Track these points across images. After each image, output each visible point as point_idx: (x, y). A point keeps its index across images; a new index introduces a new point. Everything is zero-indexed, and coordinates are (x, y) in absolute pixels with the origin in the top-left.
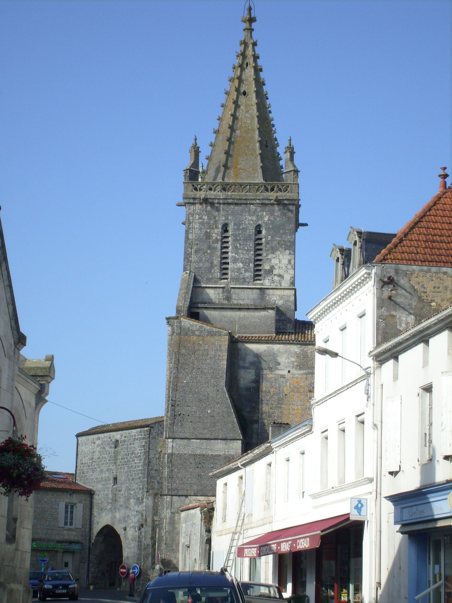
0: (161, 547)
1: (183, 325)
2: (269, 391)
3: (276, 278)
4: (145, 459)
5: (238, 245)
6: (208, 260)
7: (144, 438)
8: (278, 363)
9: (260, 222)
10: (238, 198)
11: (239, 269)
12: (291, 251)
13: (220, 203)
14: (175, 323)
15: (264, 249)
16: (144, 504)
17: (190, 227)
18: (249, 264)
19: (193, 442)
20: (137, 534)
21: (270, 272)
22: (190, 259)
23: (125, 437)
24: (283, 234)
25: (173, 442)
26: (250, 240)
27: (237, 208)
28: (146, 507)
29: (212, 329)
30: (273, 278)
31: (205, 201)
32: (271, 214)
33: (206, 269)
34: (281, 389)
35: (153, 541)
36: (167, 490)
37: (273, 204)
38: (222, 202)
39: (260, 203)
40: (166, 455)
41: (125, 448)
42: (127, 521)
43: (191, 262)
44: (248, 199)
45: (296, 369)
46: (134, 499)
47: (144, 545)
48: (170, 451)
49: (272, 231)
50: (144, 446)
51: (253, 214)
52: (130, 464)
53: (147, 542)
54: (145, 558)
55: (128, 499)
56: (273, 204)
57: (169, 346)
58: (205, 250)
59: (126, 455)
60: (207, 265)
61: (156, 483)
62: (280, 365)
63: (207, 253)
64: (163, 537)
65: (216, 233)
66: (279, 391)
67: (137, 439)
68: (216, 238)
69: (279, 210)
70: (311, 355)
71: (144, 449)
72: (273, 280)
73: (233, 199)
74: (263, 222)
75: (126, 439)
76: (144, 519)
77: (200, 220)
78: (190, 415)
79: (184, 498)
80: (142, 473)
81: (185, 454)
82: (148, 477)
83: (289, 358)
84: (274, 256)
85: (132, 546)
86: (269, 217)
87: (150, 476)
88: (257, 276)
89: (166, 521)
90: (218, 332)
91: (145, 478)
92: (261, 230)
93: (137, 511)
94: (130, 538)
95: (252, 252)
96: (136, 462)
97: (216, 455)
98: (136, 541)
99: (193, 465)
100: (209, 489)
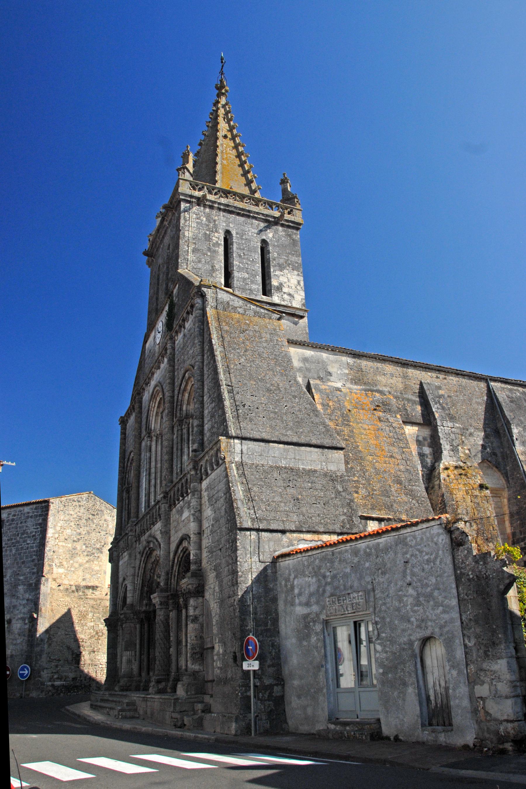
0: (247, 626)
2: (328, 404)
3: (285, 296)
6: (208, 262)
20: (27, 626)
21: (279, 288)
23: (14, 515)
26: (255, 252)
30: (282, 296)
32: (275, 232)
40: (233, 465)
41: (13, 528)
42: (12, 612)
45: (352, 383)
46: (25, 585)
52: (20, 545)
55: (16, 586)
59: (14, 535)
62: (331, 376)
63: (207, 255)
65: (219, 237)
66: (340, 405)
67: (31, 517)
69: (283, 231)
71: (41, 528)
75: (15, 518)
78: (261, 408)
81: (263, 465)
83: (341, 369)
84: (282, 273)
85: (19, 641)
88: (266, 290)
93: (28, 600)
94: (16, 633)
96: (29, 542)
97: (310, 471)
98: (24, 635)
99: (280, 483)
100: (317, 521)
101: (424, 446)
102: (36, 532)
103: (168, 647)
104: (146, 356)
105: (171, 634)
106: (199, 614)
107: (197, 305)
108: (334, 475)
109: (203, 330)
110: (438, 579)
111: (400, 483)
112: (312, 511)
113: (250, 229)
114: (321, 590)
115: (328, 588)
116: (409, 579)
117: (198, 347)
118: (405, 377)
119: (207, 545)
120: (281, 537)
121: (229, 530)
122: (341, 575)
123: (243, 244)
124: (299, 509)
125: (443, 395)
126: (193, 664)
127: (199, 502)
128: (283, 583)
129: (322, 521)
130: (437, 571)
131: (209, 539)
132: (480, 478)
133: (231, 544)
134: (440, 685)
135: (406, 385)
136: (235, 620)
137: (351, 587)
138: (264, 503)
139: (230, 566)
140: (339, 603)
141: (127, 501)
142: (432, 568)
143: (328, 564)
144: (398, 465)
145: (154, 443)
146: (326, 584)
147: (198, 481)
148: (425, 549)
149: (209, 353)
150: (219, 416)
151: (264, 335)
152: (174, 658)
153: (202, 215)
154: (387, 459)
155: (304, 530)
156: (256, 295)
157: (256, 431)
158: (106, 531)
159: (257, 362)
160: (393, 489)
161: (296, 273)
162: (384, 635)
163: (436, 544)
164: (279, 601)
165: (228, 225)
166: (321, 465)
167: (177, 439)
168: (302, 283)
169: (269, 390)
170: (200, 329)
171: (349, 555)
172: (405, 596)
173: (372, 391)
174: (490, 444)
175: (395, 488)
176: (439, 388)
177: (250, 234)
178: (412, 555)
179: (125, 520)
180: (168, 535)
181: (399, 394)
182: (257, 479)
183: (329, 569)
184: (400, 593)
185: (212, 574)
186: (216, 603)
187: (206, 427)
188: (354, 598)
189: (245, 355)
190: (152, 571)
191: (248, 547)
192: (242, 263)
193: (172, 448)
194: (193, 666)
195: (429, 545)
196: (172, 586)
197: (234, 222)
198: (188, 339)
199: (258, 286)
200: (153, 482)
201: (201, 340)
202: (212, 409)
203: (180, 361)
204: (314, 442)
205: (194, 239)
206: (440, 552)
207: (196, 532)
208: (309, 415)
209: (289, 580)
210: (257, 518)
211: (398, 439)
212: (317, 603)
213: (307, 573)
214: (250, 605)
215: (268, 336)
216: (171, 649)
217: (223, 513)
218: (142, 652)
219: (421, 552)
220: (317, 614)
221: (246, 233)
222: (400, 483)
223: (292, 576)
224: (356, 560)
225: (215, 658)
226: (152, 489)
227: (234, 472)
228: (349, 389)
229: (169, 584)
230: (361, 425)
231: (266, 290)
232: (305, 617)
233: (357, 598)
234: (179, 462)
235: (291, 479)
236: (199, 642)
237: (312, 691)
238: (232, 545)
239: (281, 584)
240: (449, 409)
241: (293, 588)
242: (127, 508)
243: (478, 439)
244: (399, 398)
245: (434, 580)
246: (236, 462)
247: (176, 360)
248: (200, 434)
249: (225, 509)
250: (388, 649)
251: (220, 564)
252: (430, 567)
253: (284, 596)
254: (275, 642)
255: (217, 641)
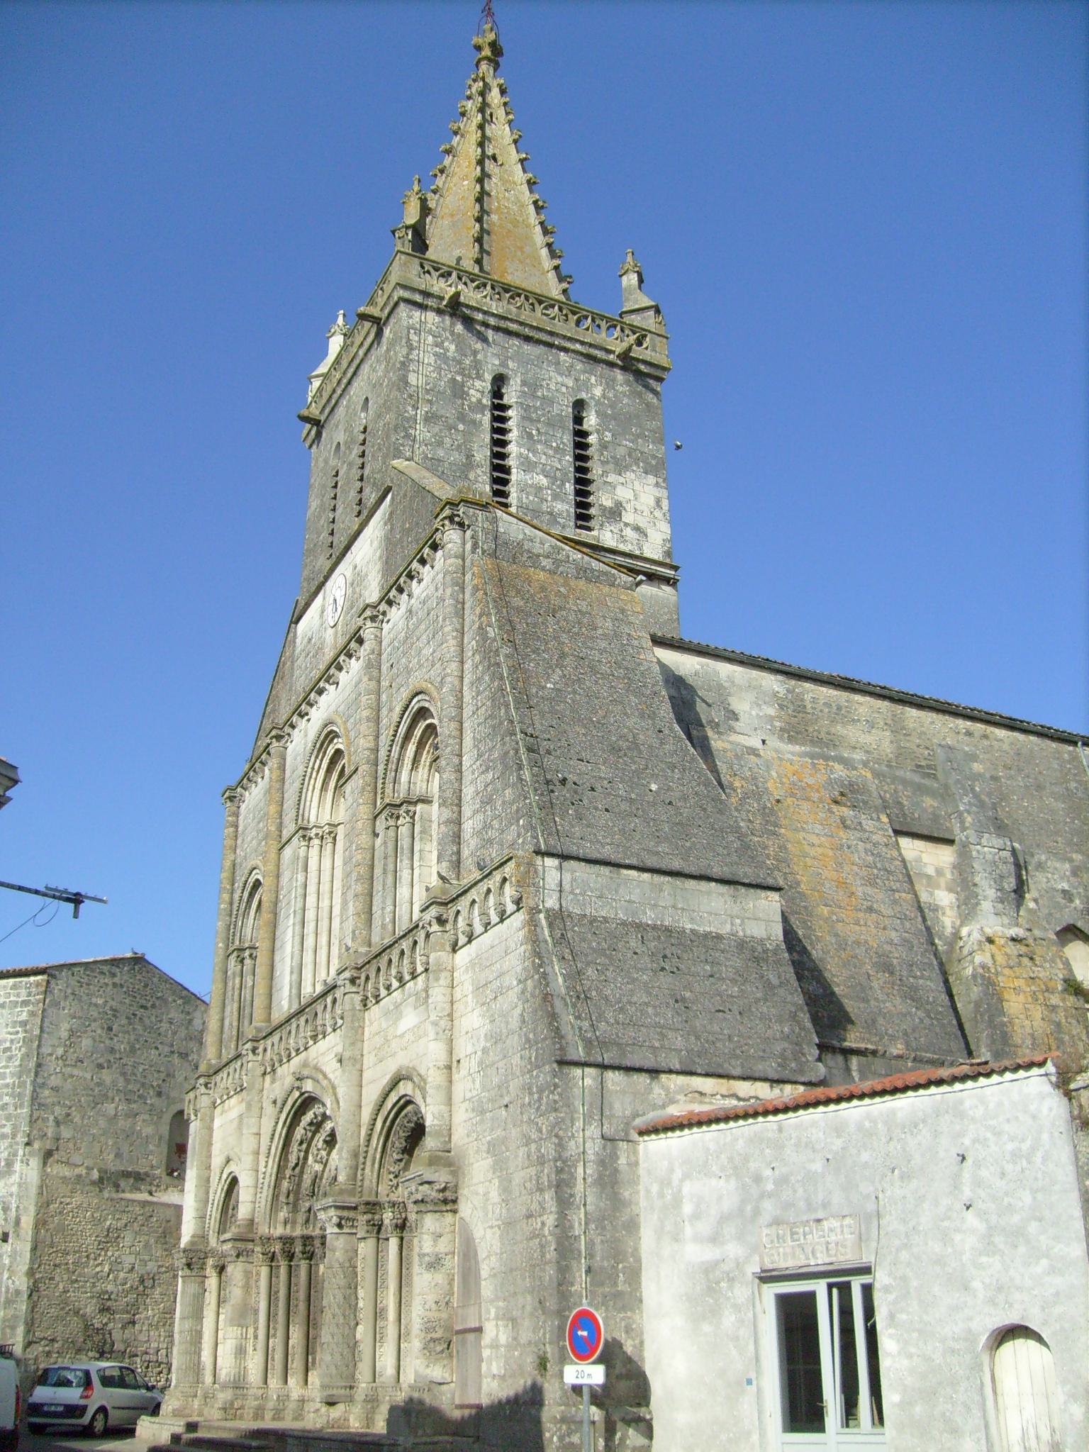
0: (572, 1285)
1: (501, 530)
3: (629, 532)
4: (27, 1056)
5: (534, 432)
6: (459, 446)
7: (25, 1003)
8: (734, 713)
9: (583, 395)
10: (535, 324)
11: (539, 489)
12: (660, 480)
13: (487, 325)
14: (480, 519)
15: (596, 458)
16: (15, 1178)
17: (411, 357)
18: (563, 484)
19: (629, 880)
21: (615, 513)
22: (412, 432)
24: (638, 436)
25: (560, 868)
27: (527, 348)
28: (20, 1185)
29: (589, 563)
30: (622, 531)
31: (452, 308)
32: (607, 384)
33: (454, 468)
34: (760, 785)
35: (32, 1281)
36: (580, 1043)
37: (611, 365)
38: (493, 323)
39: (585, 351)
40: (542, 916)
43: (414, 441)
44: (557, 335)
45: (781, 738)
47: (7, 1292)
48: (551, 902)
49: (613, 422)
50: (24, 1024)
51: (567, 373)
53: (17, 1283)
54: (8, 1331)
56: (611, 365)
57: (456, 588)
58: (450, 421)
60: (456, 457)
61: (51, 1123)
62: (737, 720)
63: (457, 430)
64: (577, 1238)
65: (479, 390)
68: (479, 401)
69: (627, 383)
70: (812, 708)
71: (26, 1031)
72: (622, 537)
73: (521, 324)
74: (591, 398)
76: (13, 1219)
77: (437, 349)
79: (643, 1079)
80: (13, 1092)
81: (606, 920)
82: (32, 1104)
83: (759, 705)
84: (622, 480)
86: (604, 391)
87: (39, 1104)
88: (583, 517)
89: (585, 1172)
90: (606, 574)
91: (22, 1106)
92: (584, 415)
95: (568, 458)
97: (706, 935)
101: (938, 887)
102: (12, 1041)
103: (352, 1324)
104: (297, 651)
105: (361, 1293)
106: (447, 1250)
107: (450, 546)
108: (759, 948)
109: (463, 603)
110: (1039, 1196)
111: (888, 968)
112: (716, 1028)
113: (552, 374)
114: (749, 1208)
115: (768, 1207)
116: (967, 1193)
117: (452, 642)
118: (897, 728)
119: (468, 1095)
120: (650, 1084)
121: (531, 1063)
122: (799, 1178)
123: (536, 409)
124: (686, 1021)
125: (980, 775)
126: (428, 1366)
127: (448, 996)
128: (655, 1189)
129: (738, 1052)
130: (1036, 1179)
131: (474, 1081)
132: (1062, 966)
133: (536, 1096)
134: (1037, 1437)
135: (900, 747)
136: (544, 1271)
137: (825, 1205)
138: (612, 1006)
139: (533, 1146)
140: (793, 1240)
141: (237, 980)
142: (1023, 1171)
143: (768, 1151)
144: (884, 928)
145: (314, 852)
146: (762, 1196)
147: (449, 948)
148: (1006, 1127)
149: (477, 658)
150: (504, 803)
151: (599, 622)
152: (365, 1348)
153: (447, 338)
154: (861, 915)
155: (699, 1071)
156: (563, 527)
157: (591, 842)
158: (172, 1045)
159: (587, 683)
160: (875, 984)
161: (651, 479)
162: (904, 1317)
163: (1034, 1117)
164: (642, 1230)
165: (503, 364)
166: (732, 924)
167: (386, 847)
168: (665, 504)
169: (615, 750)
170: (457, 601)
171: (821, 1134)
172: (957, 1230)
173: (827, 758)
174: (1081, 890)
175: (879, 981)
176: (973, 758)
177: (553, 387)
178: (975, 1141)
179: (231, 1024)
180: (358, 1066)
181: (884, 768)
182: (594, 950)
183: (771, 1163)
184: (946, 1224)
185: (482, 1162)
186: (491, 1227)
187: (468, 826)
188: (831, 1230)
189: (562, 667)
190: (304, 1146)
191: (576, 1103)
192: (535, 452)
193: (372, 867)
194: (428, 1371)
195: (1017, 1118)
196: (367, 1183)
197: (517, 357)
198: (420, 622)
199: (565, 507)
200: (309, 942)
201: (458, 627)
202: (486, 786)
203: (395, 670)
204: (716, 871)
205: (428, 391)
206: (1045, 1136)
207: (441, 1064)
208: (705, 810)
209: (669, 1184)
210: (597, 1038)
211: (886, 870)
212: (740, 1237)
213: (714, 1168)
214: (580, 1235)
215: (609, 624)
216: (360, 1328)
217: (514, 1023)
218: (272, 1332)
219: (998, 1134)
220: (738, 1264)
221: (544, 383)
222: (888, 968)
223: (678, 1174)
224: (838, 1143)
225: (486, 1353)
226: (308, 957)
227: (543, 934)
228: (776, 751)
229: (359, 1177)
230: (802, 834)
231: (583, 517)
232: (708, 1269)
233: (839, 1230)
234: (389, 901)
235: (668, 953)
236: (444, 1315)
237: (723, 1437)
238: (540, 1099)
239: (648, 1191)
240: (994, 807)
241: (677, 1201)
242: (236, 997)
243: (1055, 877)
244: (884, 776)
245: (1027, 1198)
246: (548, 911)
247: (384, 668)
248: (453, 842)
249: (522, 1015)
250: (913, 1350)
251: (504, 1140)
252: (1018, 1168)
253: (655, 1217)
254: (634, 1322)
255: (493, 1315)
